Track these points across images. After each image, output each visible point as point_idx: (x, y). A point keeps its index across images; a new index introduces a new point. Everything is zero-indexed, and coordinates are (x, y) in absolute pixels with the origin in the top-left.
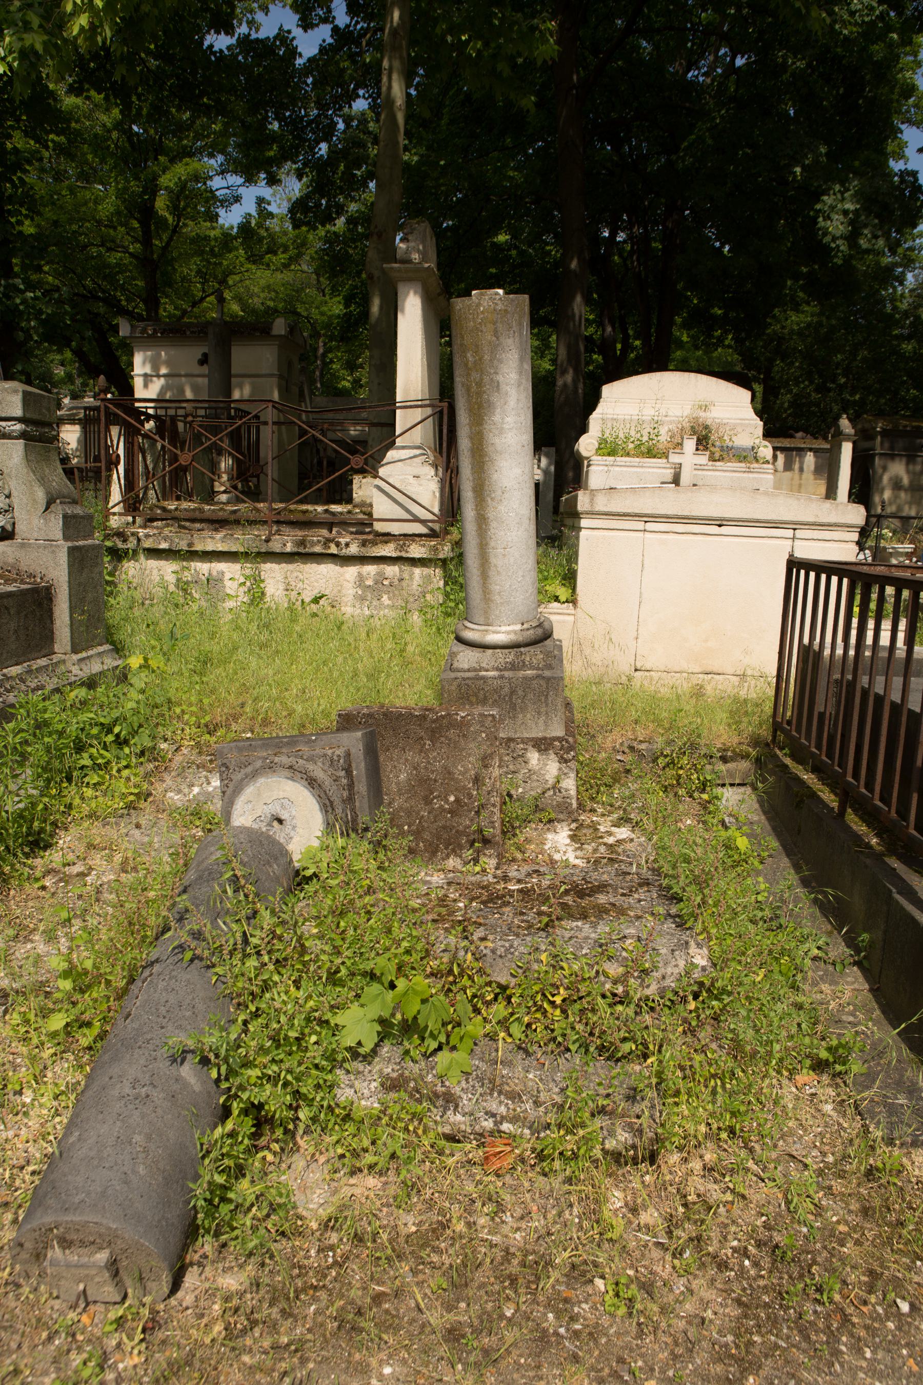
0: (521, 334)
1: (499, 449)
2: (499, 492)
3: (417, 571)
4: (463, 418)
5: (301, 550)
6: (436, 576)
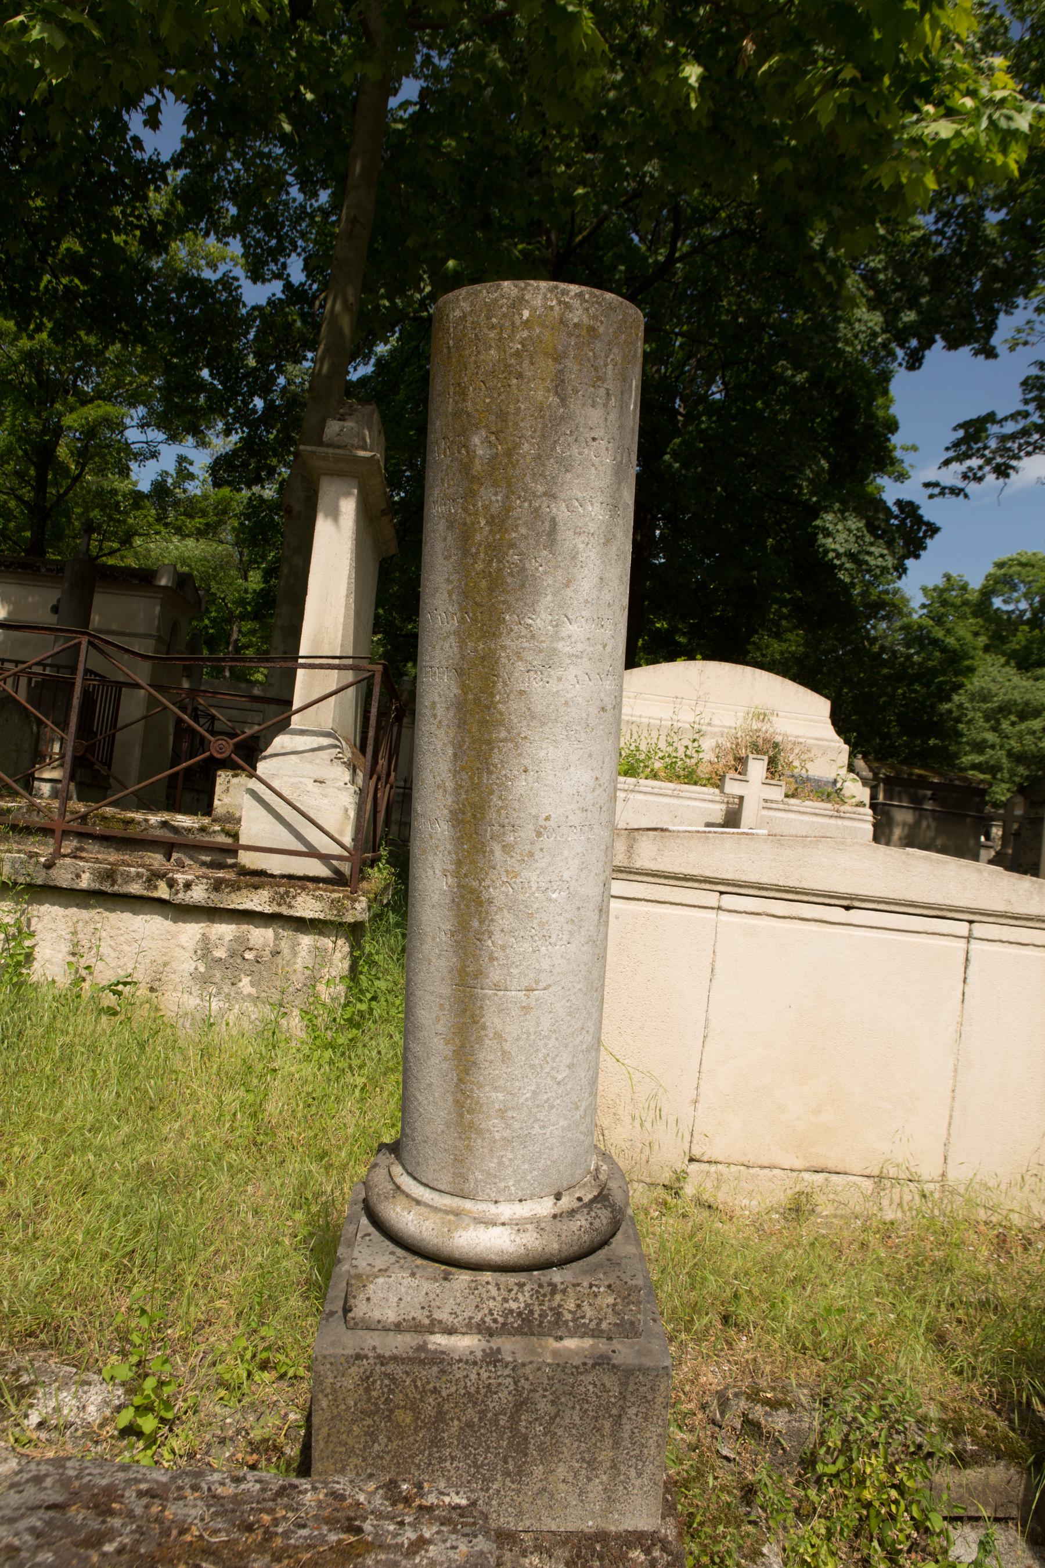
0: (623, 407)
1: (539, 707)
2: (527, 832)
3: (306, 941)
4: (441, 617)
5: (107, 887)
6: (338, 953)
